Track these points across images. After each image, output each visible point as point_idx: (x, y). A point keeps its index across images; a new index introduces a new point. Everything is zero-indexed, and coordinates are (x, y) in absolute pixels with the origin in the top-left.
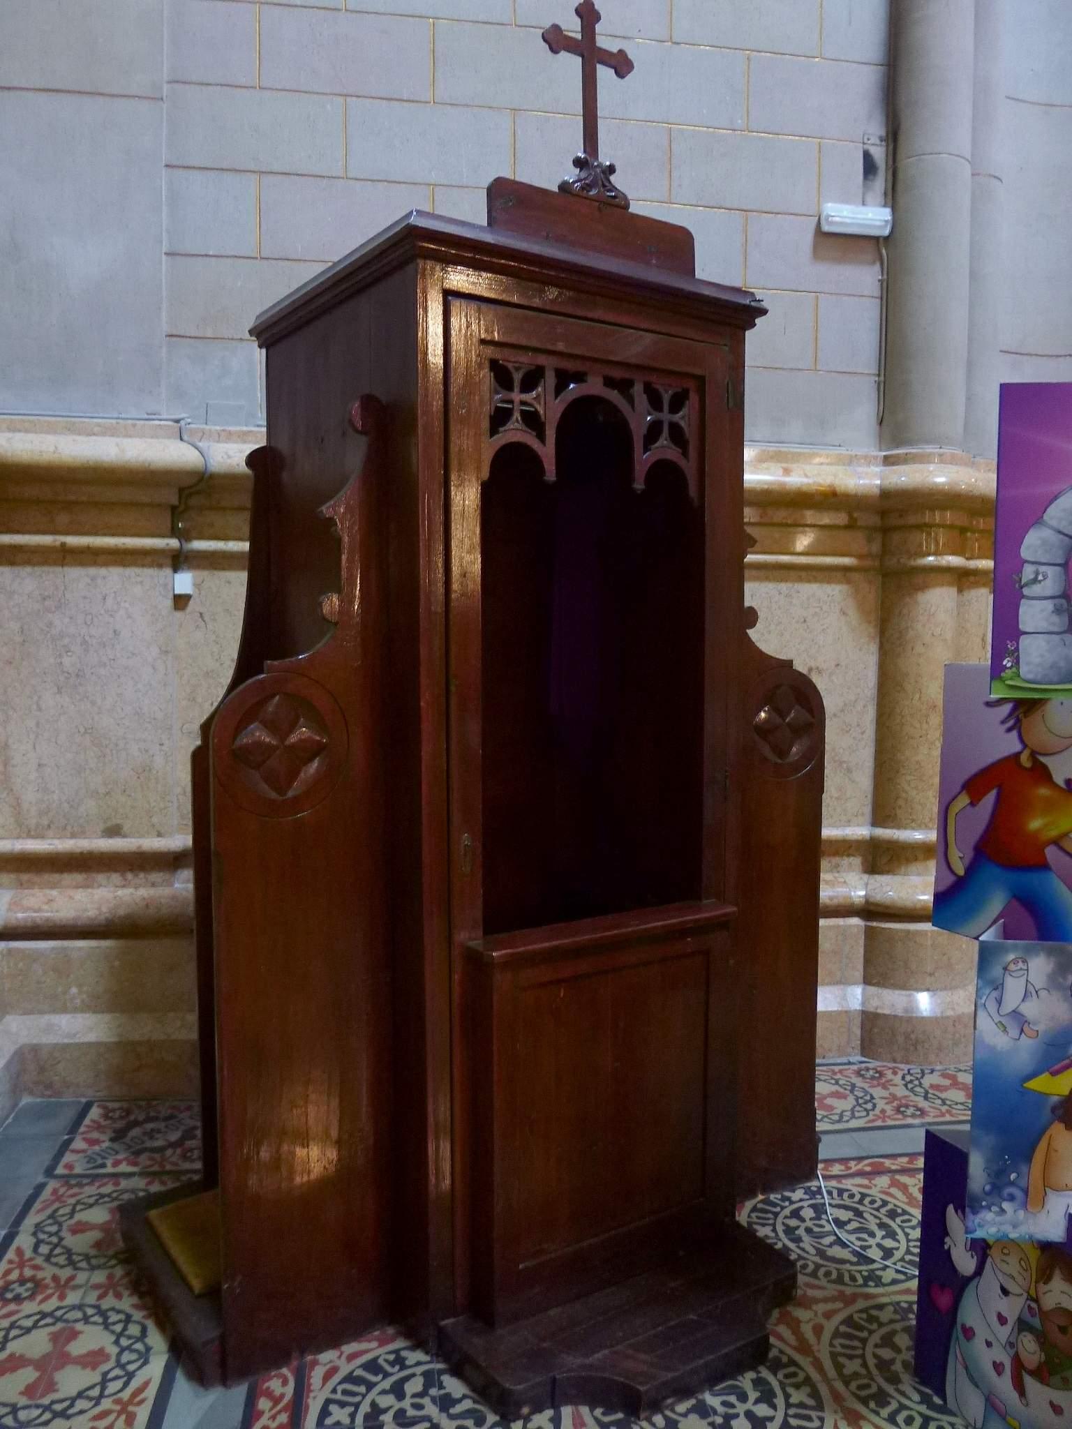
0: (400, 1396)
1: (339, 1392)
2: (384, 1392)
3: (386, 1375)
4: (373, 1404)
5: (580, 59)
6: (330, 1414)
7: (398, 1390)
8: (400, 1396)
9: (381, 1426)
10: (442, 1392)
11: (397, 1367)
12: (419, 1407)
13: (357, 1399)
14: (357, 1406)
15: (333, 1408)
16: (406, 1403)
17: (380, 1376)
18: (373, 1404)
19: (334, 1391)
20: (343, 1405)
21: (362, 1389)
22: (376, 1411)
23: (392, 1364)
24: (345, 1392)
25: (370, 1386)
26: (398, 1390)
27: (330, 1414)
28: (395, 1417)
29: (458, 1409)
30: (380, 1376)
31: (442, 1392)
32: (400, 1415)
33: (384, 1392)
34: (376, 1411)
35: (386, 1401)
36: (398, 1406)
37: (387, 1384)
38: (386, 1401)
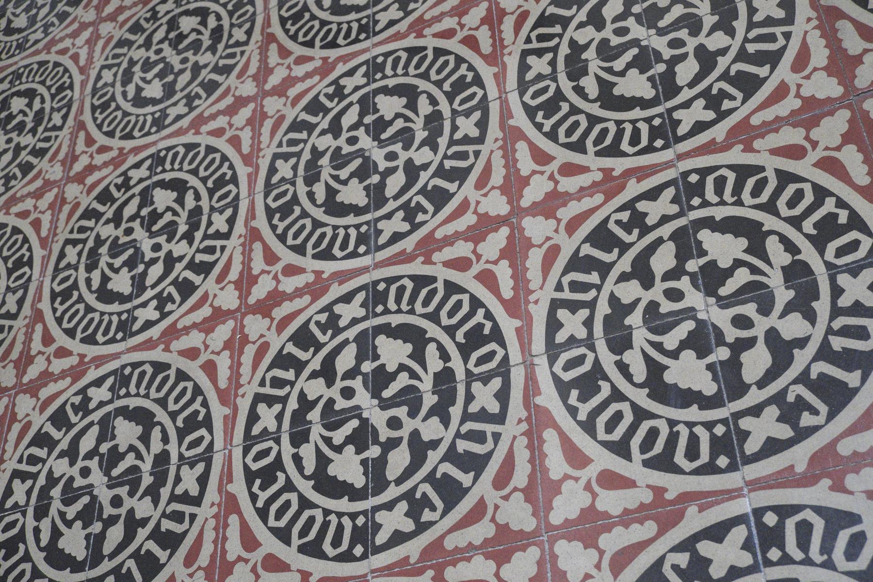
0: (701, 52)
1: (780, 37)
2: (723, 52)
3: (725, 76)
4: (573, 43)
5: (675, 460)
6: (530, 68)
7: (707, 59)
8: (701, 52)
9: (714, 10)
10: (650, 73)
11: (714, 91)
12: (676, 43)
13: (752, 35)
14: (555, 50)
15: (531, 60)
16: (607, 32)
17: (732, 73)
18: (573, 43)
19: (787, 36)
20: (539, 53)
21: (751, 48)
22: (725, 26)
23: (723, 95)
24: (772, 38)
25: (742, 56)
26: (707, 59)
27: (530, 68)
28: (332, 159)
29: (628, 56)
30: (732, 73)
31: (650, 73)
32: (693, 24)
33: (723, 52)
34: (725, 26)
35: (717, 41)
36: (701, 39)
37: (723, 63)
38: (717, 41)
